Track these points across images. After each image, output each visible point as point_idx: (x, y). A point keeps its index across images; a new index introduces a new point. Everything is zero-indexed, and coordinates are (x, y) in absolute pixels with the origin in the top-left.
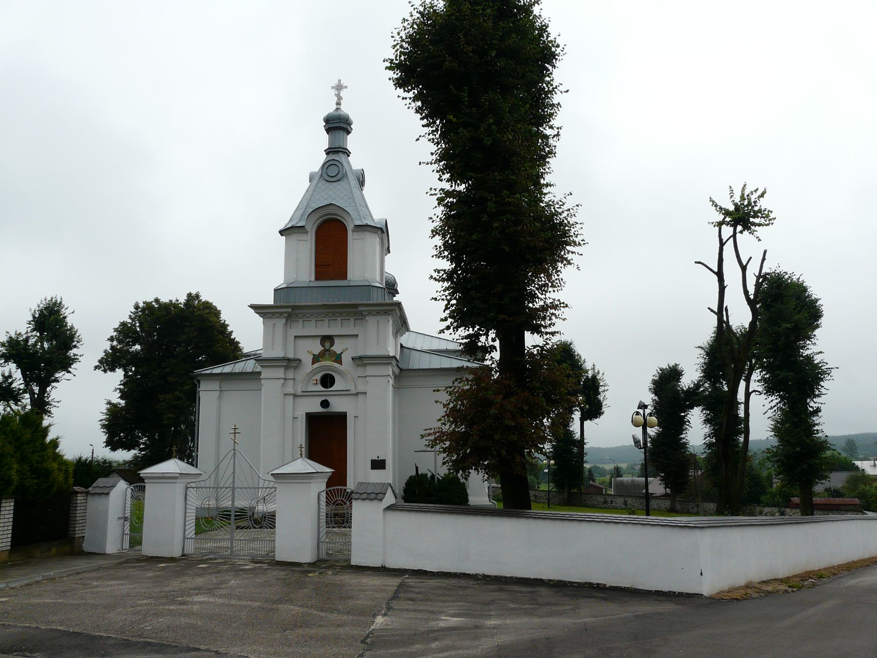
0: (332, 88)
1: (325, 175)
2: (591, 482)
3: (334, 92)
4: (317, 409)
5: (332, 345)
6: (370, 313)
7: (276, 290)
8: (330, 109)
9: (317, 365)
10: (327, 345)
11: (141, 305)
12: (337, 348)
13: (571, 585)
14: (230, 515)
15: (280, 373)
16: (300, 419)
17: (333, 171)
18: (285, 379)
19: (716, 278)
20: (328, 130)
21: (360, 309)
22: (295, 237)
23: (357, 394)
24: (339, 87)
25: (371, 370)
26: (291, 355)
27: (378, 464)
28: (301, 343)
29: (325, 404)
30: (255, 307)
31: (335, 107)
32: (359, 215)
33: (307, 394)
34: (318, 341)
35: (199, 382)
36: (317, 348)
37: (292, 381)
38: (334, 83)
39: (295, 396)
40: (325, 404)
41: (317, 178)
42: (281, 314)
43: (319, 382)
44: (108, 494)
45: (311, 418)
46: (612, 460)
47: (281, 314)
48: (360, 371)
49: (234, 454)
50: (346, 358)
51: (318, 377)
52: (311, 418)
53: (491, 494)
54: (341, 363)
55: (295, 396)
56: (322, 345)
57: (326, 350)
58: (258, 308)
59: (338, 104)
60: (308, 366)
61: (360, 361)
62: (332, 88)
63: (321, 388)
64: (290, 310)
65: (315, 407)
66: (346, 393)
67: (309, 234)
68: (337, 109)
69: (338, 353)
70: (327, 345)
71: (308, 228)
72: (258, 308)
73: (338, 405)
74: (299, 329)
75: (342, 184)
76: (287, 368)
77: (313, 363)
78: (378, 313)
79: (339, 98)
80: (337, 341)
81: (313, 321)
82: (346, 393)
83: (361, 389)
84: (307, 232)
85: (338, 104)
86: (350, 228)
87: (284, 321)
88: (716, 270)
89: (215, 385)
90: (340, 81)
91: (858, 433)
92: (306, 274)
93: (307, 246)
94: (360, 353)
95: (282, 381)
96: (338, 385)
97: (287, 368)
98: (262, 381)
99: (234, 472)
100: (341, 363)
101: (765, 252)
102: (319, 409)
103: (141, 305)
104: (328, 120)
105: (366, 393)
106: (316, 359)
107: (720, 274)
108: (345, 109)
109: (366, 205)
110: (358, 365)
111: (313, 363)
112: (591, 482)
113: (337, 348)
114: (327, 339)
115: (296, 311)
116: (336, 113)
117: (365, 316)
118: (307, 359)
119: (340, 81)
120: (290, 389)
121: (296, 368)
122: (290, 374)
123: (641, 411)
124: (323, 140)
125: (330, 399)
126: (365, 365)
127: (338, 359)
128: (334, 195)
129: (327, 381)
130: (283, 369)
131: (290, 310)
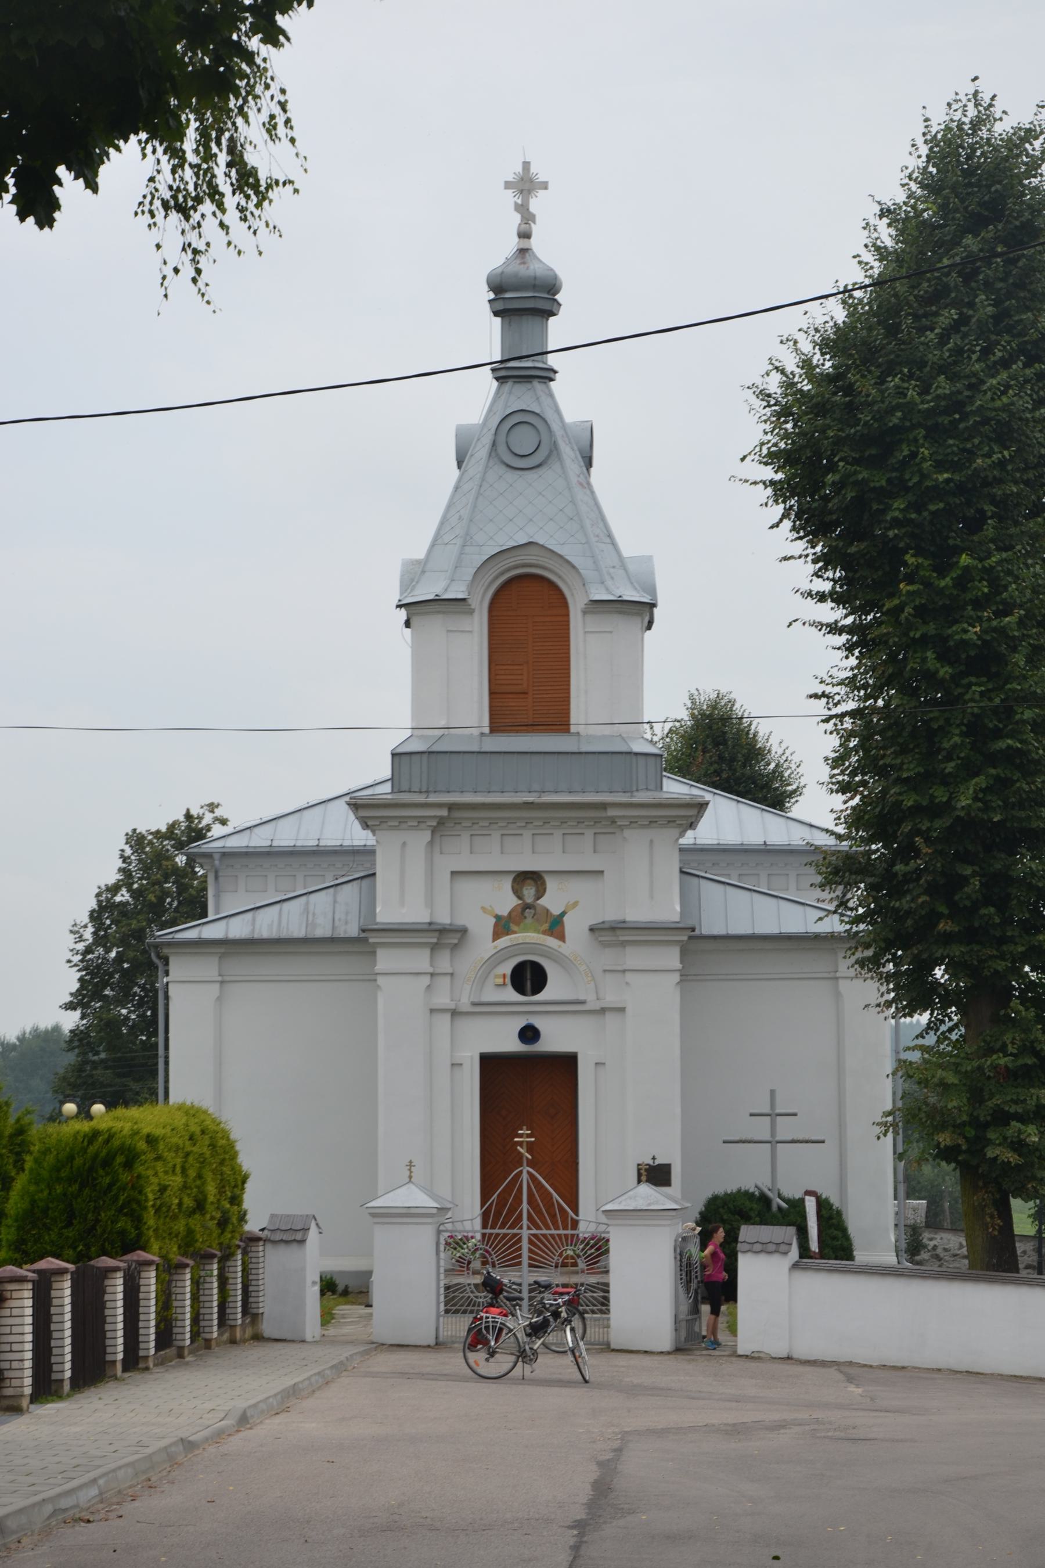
0: (508, 185)
1: (502, 449)
3: (510, 198)
4: (509, 1043)
5: (540, 893)
6: (633, 823)
8: (497, 252)
9: (504, 941)
11: (138, 831)
12: (552, 901)
13: (1021, 1377)
14: (531, 1265)
15: (420, 960)
16: (467, 1067)
17: (523, 440)
18: (432, 975)
21: (611, 812)
22: (435, 626)
23: (603, 1011)
24: (526, 185)
25: (634, 957)
26: (444, 918)
27: (657, 1175)
28: (468, 888)
29: (529, 1034)
31: (513, 243)
32: (598, 569)
33: (482, 1009)
34: (507, 884)
35: (166, 961)
36: (506, 902)
37: (448, 979)
38: (512, 170)
39: (455, 1013)
40: (529, 1034)
41: (481, 452)
42: (421, 820)
43: (508, 980)
44: (302, 1242)
45: (492, 1065)
46: (187, 1364)
47: (421, 820)
48: (608, 958)
50: (575, 926)
51: (507, 968)
52: (492, 1065)
54: (562, 937)
55: (455, 1013)
56: (517, 893)
59: (525, 235)
60: (483, 944)
61: (611, 933)
63: (511, 994)
64: (444, 813)
65: (505, 1040)
66: (573, 1007)
67: (476, 615)
68: (523, 252)
69: (556, 911)
70: (529, 892)
71: (474, 603)
73: (555, 1039)
74: (461, 853)
75: (548, 474)
76: (434, 948)
77: (496, 936)
78: (652, 822)
79: (527, 217)
80: (551, 884)
81: (496, 836)
82: (573, 1007)
83: (611, 999)
84: (471, 612)
85: (525, 235)
86: (576, 606)
87: (427, 836)
89: (207, 967)
91: (852, 1236)
92: (469, 709)
93: (469, 645)
94: (611, 915)
95: (426, 980)
97: (434, 948)
98: (381, 980)
100: (562, 937)
102: (512, 1045)
103: (138, 831)
104: (498, 286)
105: (622, 1010)
106: (502, 927)
108: (550, 252)
109: (610, 536)
110: (604, 945)
111: (496, 936)
113: (552, 901)
114: (529, 880)
115: (457, 814)
116: (516, 268)
117: (621, 828)
118: (482, 927)
120: (443, 999)
121: (455, 947)
122: (444, 963)
124: (487, 338)
125: (538, 1023)
126: (624, 944)
127: (556, 927)
128: (527, 516)
129: (529, 977)
130: (426, 953)
131: (444, 813)
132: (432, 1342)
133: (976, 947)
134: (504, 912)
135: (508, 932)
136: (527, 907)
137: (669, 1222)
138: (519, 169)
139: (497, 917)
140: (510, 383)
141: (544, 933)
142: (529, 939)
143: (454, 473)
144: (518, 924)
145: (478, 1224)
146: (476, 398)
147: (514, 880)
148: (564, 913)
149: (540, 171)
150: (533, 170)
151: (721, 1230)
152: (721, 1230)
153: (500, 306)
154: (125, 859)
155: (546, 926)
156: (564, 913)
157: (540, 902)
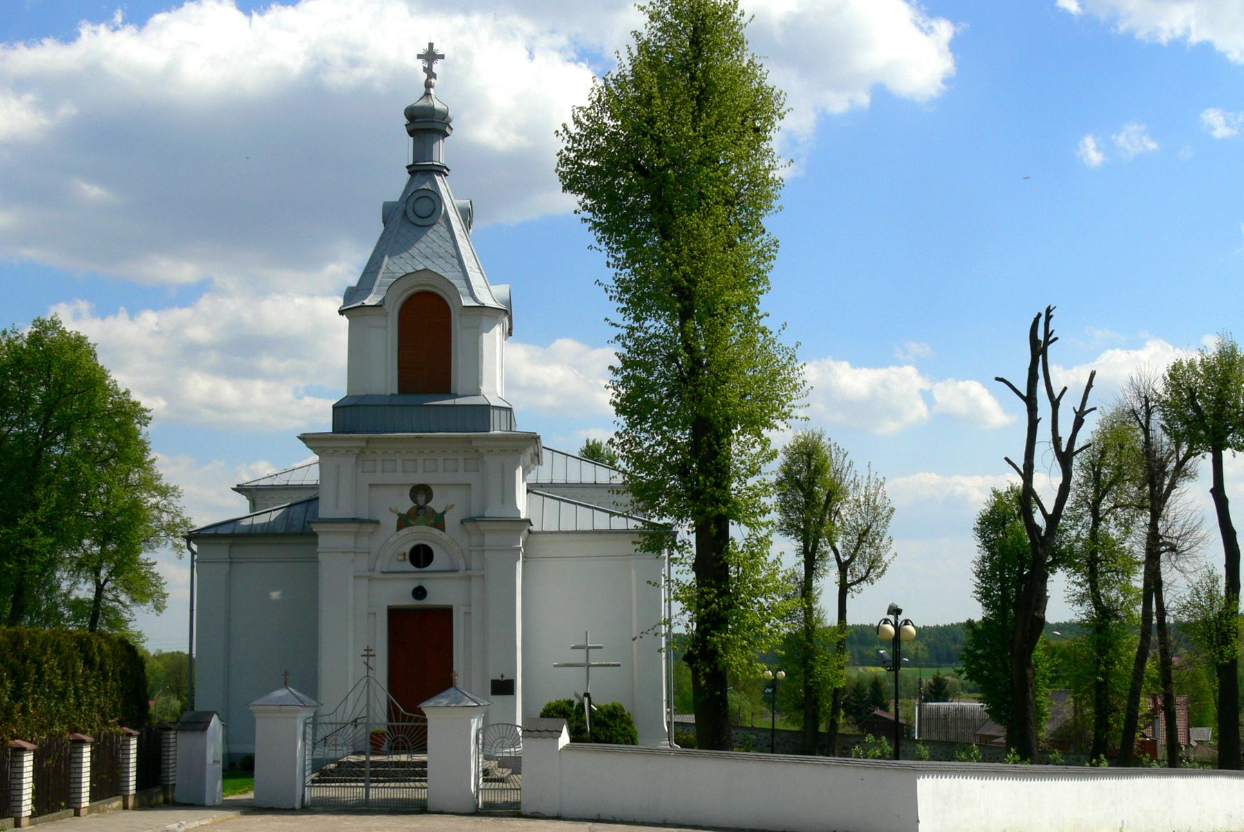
0: (419, 56)
2: (878, 712)
3: (421, 64)
7: (334, 407)
8: (414, 97)
10: (421, 499)
12: (436, 505)
15: (347, 541)
19: (1023, 406)
20: (411, 133)
29: (420, 593)
30: (305, 438)
36: (406, 505)
38: (423, 48)
39: (370, 579)
40: (420, 593)
43: (407, 557)
45: (396, 616)
49: (368, 682)
50: (451, 520)
52: (396, 616)
53: (676, 734)
54: (442, 528)
57: (419, 508)
58: (309, 439)
59: (428, 86)
62: (419, 56)
63: (408, 566)
69: (439, 511)
70: (421, 499)
72: (309, 439)
73: (438, 595)
76: (357, 534)
77: (399, 527)
79: (430, 74)
80: (436, 492)
87: (353, 460)
88: (1025, 394)
90: (431, 45)
92: (384, 380)
96: (438, 561)
97: (357, 534)
99: (368, 705)
100: (442, 528)
101: (1007, 459)
102: (408, 601)
106: (403, 522)
107: (1031, 401)
111: (399, 527)
112: (878, 712)
113: (436, 505)
114: (421, 491)
116: (423, 103)
119: (431, 45)
123: (892, 618)
125: (427, 586)
129: (421, 556)
132: (298, 805)
133: (703, 414)
134: (405, 511)
135: (408, 525)
136: (419, 508)
137: (261, 483)
138: (427, 47)
139: (400, 515)
140: (418, 176)
141: (431, 525)
142: (420, 534)
143: (382, 228)
144: (414, 519)
145: (385, 720)
146: (395, 185)
147: (412, 491)
148: (444, 512)
149: (438, 49)
150: (435, 48)
151: (560, 746)
152: (560, 746)
153: (412, 127)
154: (164, 492)
155: (432, 521)
156: (444, 512)
157: (429, 504)
